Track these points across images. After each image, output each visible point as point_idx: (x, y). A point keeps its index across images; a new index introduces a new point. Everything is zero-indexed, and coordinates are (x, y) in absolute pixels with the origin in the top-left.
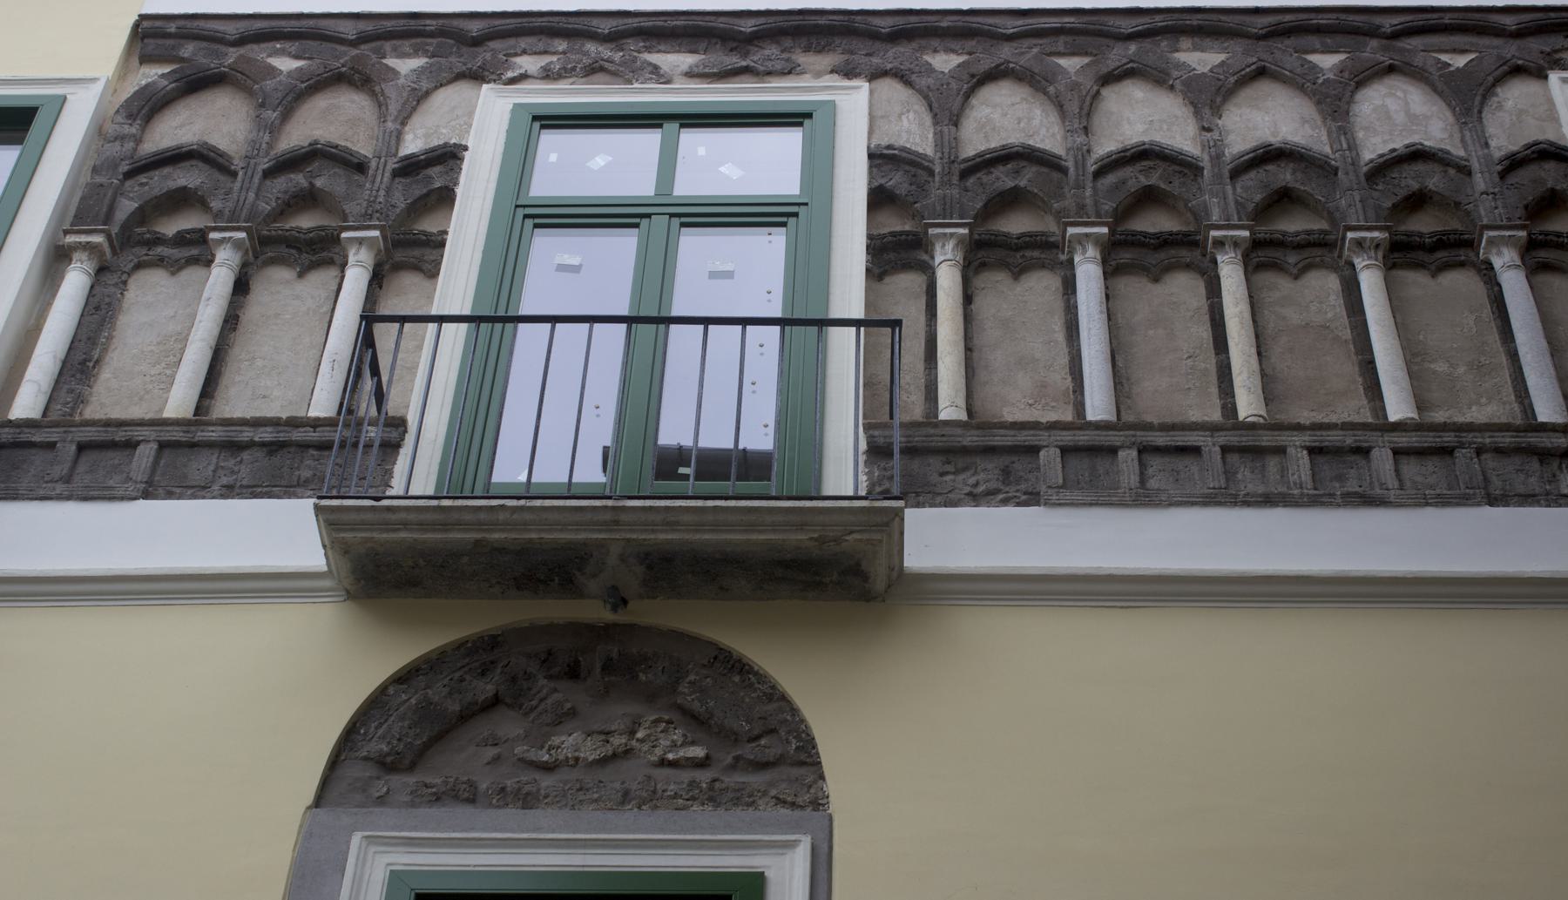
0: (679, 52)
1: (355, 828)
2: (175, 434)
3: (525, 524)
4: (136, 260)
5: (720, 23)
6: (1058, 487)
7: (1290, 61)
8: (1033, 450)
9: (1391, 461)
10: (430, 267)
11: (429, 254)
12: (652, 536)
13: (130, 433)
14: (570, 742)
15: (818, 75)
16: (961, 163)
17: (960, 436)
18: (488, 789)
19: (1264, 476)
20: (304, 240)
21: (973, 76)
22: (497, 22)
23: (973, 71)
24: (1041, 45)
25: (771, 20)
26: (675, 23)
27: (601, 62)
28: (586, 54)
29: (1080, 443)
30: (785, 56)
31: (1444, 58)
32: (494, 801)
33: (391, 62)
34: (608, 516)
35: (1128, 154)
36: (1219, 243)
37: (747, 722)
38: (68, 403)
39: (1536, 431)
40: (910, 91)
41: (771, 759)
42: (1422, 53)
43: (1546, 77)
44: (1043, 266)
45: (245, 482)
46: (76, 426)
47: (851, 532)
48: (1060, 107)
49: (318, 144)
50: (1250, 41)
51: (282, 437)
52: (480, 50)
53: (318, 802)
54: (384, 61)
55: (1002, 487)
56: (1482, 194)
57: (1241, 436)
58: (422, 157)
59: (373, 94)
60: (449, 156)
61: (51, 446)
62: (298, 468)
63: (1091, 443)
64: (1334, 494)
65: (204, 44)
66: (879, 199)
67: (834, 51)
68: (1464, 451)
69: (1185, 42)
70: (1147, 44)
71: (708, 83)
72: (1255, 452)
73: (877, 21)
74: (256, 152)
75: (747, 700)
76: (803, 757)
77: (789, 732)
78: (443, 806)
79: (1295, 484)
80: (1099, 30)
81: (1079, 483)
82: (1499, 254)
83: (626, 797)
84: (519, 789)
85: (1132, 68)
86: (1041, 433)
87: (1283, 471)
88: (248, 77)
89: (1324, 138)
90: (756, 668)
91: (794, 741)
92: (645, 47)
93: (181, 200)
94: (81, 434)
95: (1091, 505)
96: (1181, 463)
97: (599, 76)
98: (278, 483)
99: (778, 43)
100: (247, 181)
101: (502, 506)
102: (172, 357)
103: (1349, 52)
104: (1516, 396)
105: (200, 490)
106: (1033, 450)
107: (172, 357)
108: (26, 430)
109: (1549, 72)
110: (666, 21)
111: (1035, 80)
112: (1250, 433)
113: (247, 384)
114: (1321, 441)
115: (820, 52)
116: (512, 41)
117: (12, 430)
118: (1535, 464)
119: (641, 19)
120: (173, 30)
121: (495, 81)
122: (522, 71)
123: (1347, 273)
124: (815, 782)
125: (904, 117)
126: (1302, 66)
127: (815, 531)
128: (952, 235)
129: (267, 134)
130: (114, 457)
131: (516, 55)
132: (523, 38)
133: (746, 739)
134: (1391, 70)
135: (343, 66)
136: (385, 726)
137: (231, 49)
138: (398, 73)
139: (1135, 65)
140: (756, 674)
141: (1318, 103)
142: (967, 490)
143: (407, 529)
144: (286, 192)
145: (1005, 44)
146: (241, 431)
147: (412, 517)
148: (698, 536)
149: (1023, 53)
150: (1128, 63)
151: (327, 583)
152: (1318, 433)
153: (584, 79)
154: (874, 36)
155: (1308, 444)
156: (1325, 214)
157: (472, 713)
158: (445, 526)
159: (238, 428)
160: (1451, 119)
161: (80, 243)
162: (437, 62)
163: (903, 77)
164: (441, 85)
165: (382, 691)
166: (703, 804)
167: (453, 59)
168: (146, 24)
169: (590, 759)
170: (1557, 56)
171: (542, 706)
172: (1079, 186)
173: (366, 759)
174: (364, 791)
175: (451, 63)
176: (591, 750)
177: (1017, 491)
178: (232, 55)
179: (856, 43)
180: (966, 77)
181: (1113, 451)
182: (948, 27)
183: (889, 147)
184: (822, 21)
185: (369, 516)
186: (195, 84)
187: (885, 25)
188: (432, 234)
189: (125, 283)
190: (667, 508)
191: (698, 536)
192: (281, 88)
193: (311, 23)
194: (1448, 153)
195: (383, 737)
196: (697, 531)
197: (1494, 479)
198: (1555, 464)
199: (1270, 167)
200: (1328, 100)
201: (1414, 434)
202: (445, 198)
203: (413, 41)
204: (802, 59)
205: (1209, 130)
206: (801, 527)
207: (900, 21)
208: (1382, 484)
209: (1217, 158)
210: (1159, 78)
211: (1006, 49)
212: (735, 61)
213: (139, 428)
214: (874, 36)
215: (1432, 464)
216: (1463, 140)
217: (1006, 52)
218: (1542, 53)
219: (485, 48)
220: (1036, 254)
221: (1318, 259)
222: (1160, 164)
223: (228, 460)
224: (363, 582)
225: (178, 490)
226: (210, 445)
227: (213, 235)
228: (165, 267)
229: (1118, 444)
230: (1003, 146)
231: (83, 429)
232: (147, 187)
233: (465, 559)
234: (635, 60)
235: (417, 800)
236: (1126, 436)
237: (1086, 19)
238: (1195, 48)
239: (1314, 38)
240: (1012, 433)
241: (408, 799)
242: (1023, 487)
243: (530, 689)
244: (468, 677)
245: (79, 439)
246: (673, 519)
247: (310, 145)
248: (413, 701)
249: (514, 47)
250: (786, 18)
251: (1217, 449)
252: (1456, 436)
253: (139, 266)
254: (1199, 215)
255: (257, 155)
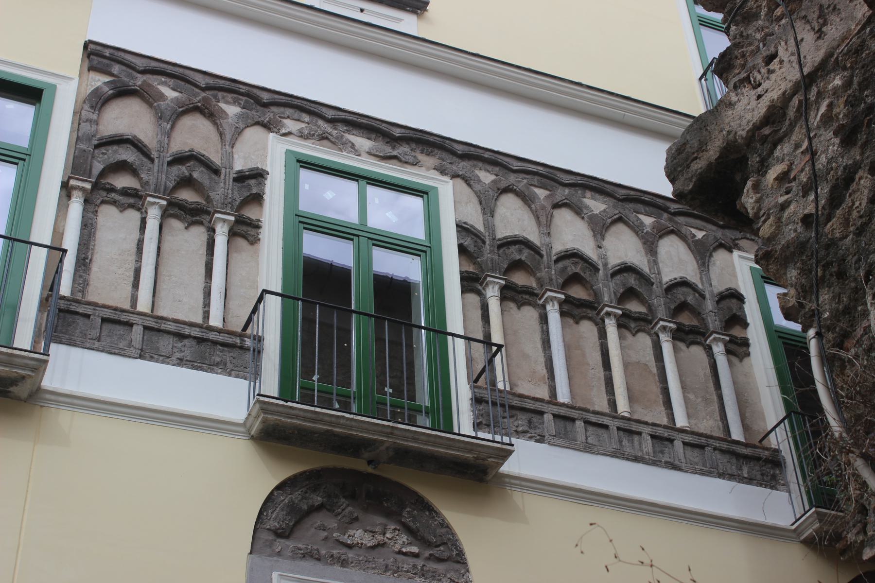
0: (362, 137)
1: (272, 570)
2: (151, 322)
3: (351, 427)
4: (101, 199)
5: (383, 127)
6: (554, 436)
7: (632, 216)
8: (541, 413)
9: (682, 449)
10: (252, 239)
11: (252, 231)
12: (406, 443)
13: (128, 317)
14: (358, 535)
15: (428, 169)
16: (497, 241)
17: (511, 399)
18: (325, 554)
19: (633, 446)
20: (190, 208)
21: (499, 189)
22: (276, 96)
23: (499, 186)
24: (527, 179)
25: (407, 131)
26: (362, 121)
27: (327, 134)
28: (319, 127)
29: (561, 414)
30: (413, 154)
31: (694, 231)
32: (329, 561)
33: (222, 105)
34: (389, 430)
35: (568, 253)
36: (608, 314)
37: (435, 537)
38: (80, 284)
39: (736, 444)
40: (470, 190)
41: (446, 558)
42: (685, 227)
43: (732, 252)
44: (530, 304)
45: (188, 358)
46: (100, 307)
47: (491, 457)
48: (537, 218)
49: (193, 151)
50: (615, 201)
51: (205, 335)
52: (267, 110)
53: (251, 553)
54: (219, 104)
55: (529, 430)
56: (710, 311)
57: (624, 423)
58: (247, 173)
59: (215, 124)
60: (259, 175)
61: (88, 316)
62: (213, 355)
63: (565, 415)
64: (661, 461)
65: (124, 68)
66: (462, 250)
67: (435, 156)
68: (709, 448)
69: (588, 194)
70: (572, 190)
71: (378, 161)
72: (630, 432)
73: (456, 146)
74: (162, 149)
75: (433, 525)
76: (459, 559)
77: (452, 545)
78: (307, 560)
79: (646, 453)
80: (553, 178)
81: (560, 434)
82: (717, 345)
83: (387, 568)
84: (340, 557)
85: (567, 203)
86: (544, 405)
87: (640, 444)
88: (150, 96)
89: (646, 263)
90: (435, 509)
91: (455, 550)
92: (347, 130)
93: (122, 167)
94: (102, 313)
95: (567, 448)
96: (601, 431)
97: (325, 142)
98: (205, 362)
99: (408, 144)
100: (161, 167)
101: (343, 416)
102: (127, 265)
103: (655, 218)
104: (721, 418)
105: (165, 358)
106: (541, 413)
107: (127, 265)
108: (74, 304)
109: (734, 250)
110: (358, 118)
111: (527, 199)
112: (628, 422)
113: (170, 291)
114: (656, 432)
115: (428, 155)
116: (282, 109)
117: (66, 302)
118: (734, 461)
119: (347, 114)
120: (107, 54)
121: (276, 133)
122: (290, 130)
123: (655, 338)
124: (465, 573)
125: (468, 205)
126: (637, 221)
127: (475, 454)
128: (498, 283)
129: (166, 138)
130: (120, 330)
131: (284, 118)
132: (288, 109)
133: (434, 545)
134: (672, 232)
135: (199, 102)
136: (275, 513)
137: (139, 75)
138: (227, 115)
139: (568, 201)
140: (435, 512)
141: (644, 243)
142: (515, 429)
143: (297, 418)
144: (178, 177)
145: (512, 174)
146: (184, 328)
147: (301, 413)
148: (425, 447)
149: (520, 182)
150: (565, 199)
151: (242, 429)
152: (654, 428)
153: (318, 142)
154: (453, 153)
155: (651, 433)
156: (647, 305)
157: (314, 510)
158: (315, 421)
159: (182, 326)
160: (696, 266)
161: (79, 186)
162: (247, 113)
163: (467, 181)
164: (248, 126)
165: (272, 493)
166: (420, 577)
167: (253, 112)
168: (91, 46)
169: (369, 545)
170: (737, 242)
171: (344, 513)
172: (549, 267)
173: (269, 529)
174: (271, 547)
175: (253, 115)
176: (368, 540)
177: (535, 433)
178: (140, 79)
179: (444, 155)
180: (496, 189)
181: (573, 420)
182: (487, 158)
183: (465, 223)
184: (431, 139)
185: (281, 409)
186: (122, 92)
187: (460, 149)
188: (252, 220)
189: (97, 211)
190: (416, 432)
191: (425, 447)
192: (169, 109)
193: (181, 70)
194: (697, 286)
195: (275, 519)
196: (426, 444)
197: (720, 464)
198: (741, 461)
199: (625, 274)
200: (648, 243)
201: (690, 436)
202: (257, 199)
203: (233, 95)
204: (421, 157)
205: (600, 247)
206: (470, 451)
207: (466, 148)
208: (679, 460)
209: (605, 265)
210: (578, 210)
211: (512, 177)
212: (388, 150)
213: (132, 315)
214: (453, 153)
215: (697, 452)
216: (701, 278)
217: (512, 178)
218: (731, 239)
219: (269, 110)
220: (527, 297)
221: (643, 328)
222: (436, 151)
223: (177, 343)
224: (263, 434)
225: (156, 356)
226: (168, 333)
227: (149, 199)
228: (117, 207)
229: (576, 417)
230: (515, 235)
231: (102, 309)
232: (106, 156)
233: (317, 435)
234: (342, 137)
235: (295, 556)
236: (579, 414)
237: (548, 170)
238: (593, 198)
239: (641, 206)
240: (533, 402)
241: (290, 554)
242: (537, 431)
243: (337, 503)
244: (308, 491)
245: (102, 316)
246: (417, 437)
247: (190, 151)
248: (286, 501)
249: (283, 113)
250: (414, 132)
251: (615, 428)
252: (706, 440)
253: (103, 202)
254: (597, 294)
255: (163, 151)
